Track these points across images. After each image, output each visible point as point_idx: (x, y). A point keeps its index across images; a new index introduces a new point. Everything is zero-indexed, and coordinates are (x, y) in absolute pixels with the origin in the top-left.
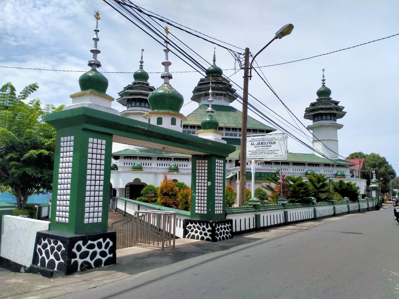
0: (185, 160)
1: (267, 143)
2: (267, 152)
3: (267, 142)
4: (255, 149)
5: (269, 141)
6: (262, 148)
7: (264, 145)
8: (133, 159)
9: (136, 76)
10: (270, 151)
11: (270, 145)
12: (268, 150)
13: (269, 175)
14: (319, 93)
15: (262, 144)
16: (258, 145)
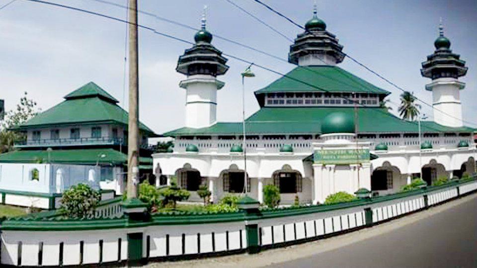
8: (255, 139)
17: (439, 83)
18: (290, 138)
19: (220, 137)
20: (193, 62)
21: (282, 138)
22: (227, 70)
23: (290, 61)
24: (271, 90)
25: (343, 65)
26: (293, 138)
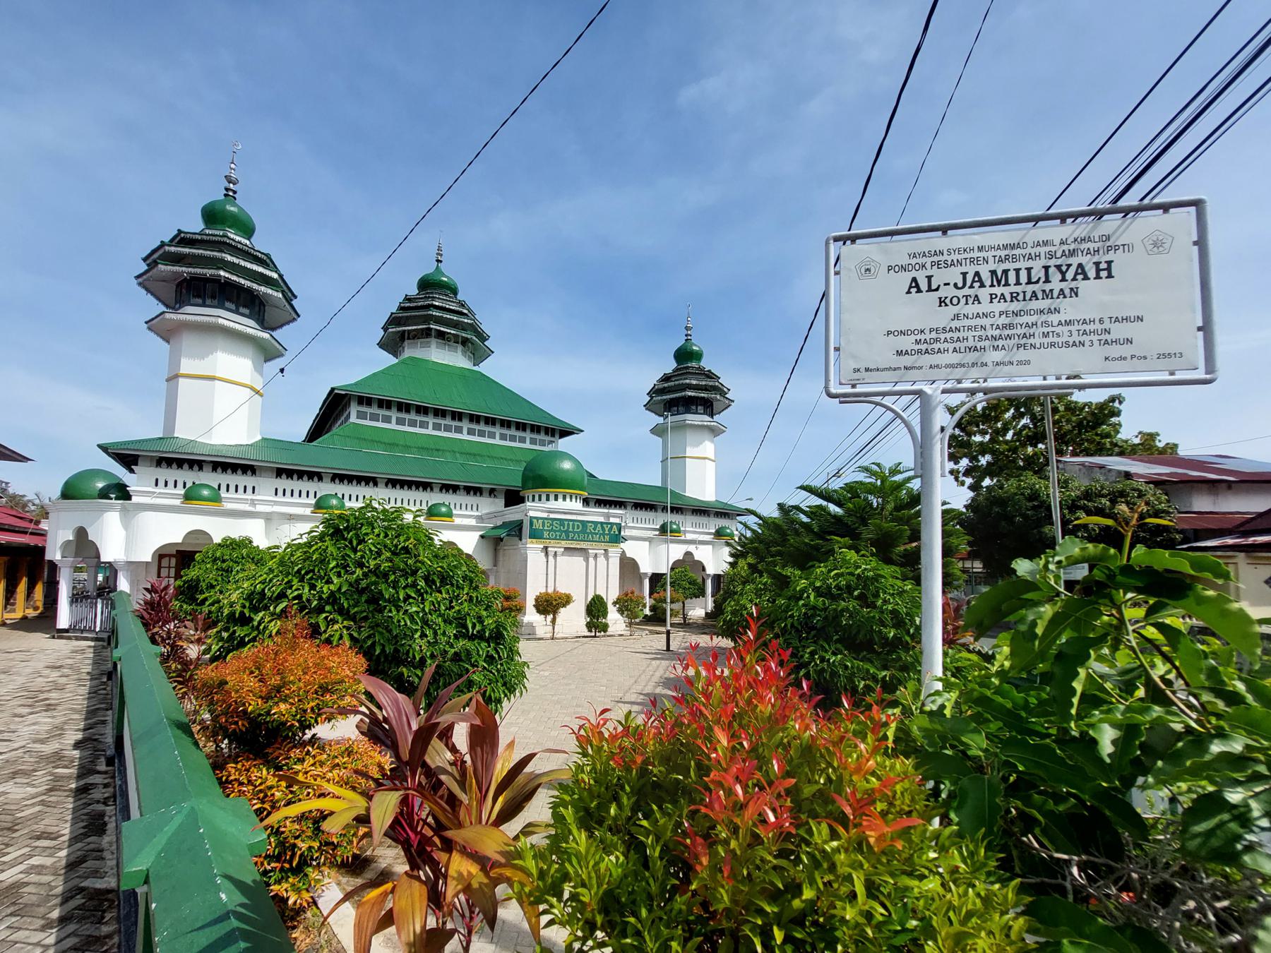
0: (367, 484)
1: (1038, 273)
2: (1046, 335)
3: (1037, 266)
4: (943, 317)
5: (1053, 262)
6: (998, 307)
7: (1018, 289)
9: (212, 215)
10: (1068, 323)
11: (1073, 285)
12: (1055, 318)
13: (603, 529)
14: (427, 285)
15: (999, 279)
16: (966, 291)
17: (221, 321)
18: (333, 480)
19: (280, 472)
20: (209, 272)
21: (425, 489)
22: (294, 319)
23: (382, 345)
24: (366, 391)
25: (486, 368)
26: (447, 491)
